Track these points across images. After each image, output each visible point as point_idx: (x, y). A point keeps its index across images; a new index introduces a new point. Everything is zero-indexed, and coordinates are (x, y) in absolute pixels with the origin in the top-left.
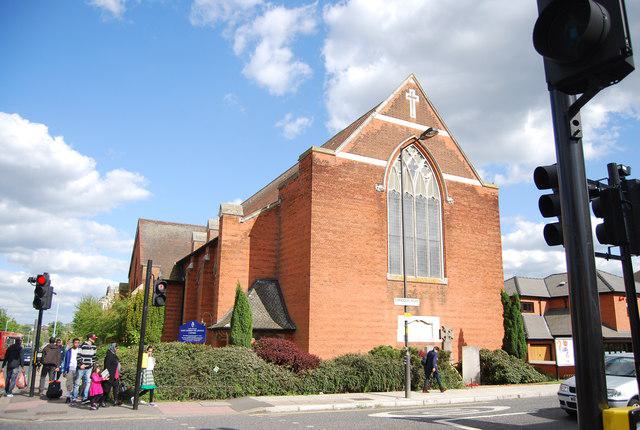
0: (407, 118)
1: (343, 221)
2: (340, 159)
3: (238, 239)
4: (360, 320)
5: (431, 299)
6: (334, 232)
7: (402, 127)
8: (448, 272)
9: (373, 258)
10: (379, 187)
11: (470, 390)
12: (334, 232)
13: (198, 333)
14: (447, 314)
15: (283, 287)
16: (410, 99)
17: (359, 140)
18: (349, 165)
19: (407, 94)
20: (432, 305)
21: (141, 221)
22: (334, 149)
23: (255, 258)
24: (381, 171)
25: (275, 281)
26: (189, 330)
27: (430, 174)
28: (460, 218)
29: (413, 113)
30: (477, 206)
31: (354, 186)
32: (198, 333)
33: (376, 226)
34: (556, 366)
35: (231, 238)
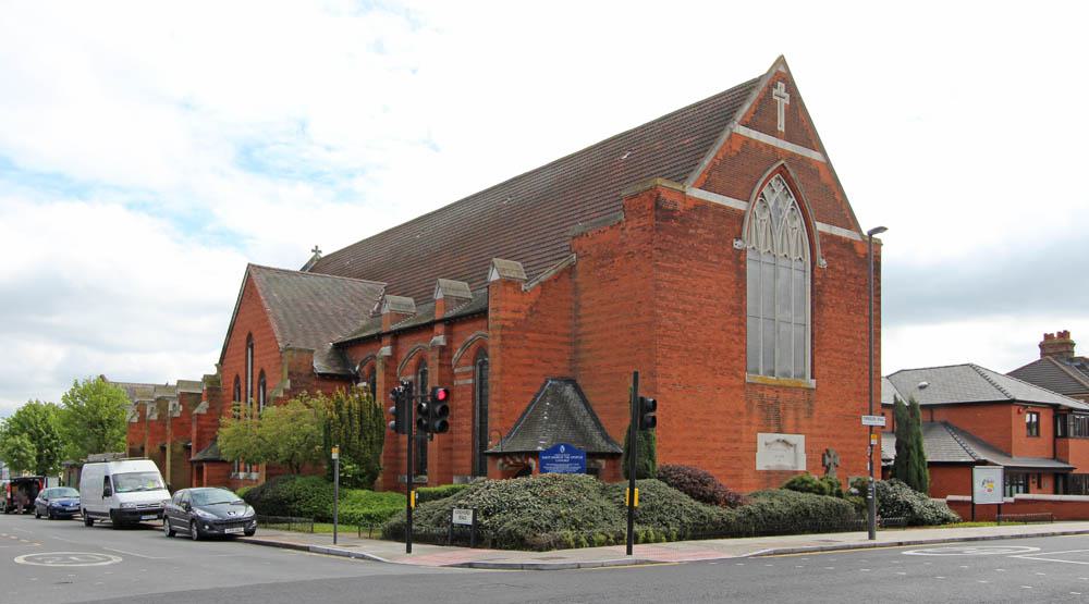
0: (773, 132)
1: (694, 295)
2: (691, 199)
3: (522, 316)
4: (714, 440)
5: (796, 410)
6: (685, 312)
7: (767, 146)
8: (816, 372)
9: (729, 350)
10: (738, 244)
11: (45, 523)
12: (685, 312)
13: (572, 461)
14: (816, 431)
15: (587, 391)
16: (778, 99)
17: (713, 167)
18: (702, 207)
19: (775, 91)
20: (797, 419)
21: (250, 266)
22: (681, 180)
24: (740, 217)
25: (572, 381)
26: (557, 457)
27: (799, 222)
28: (834, 290)
29: (781, 127)
30: (855, 271)
31: (707, 240)
32: (572, 461)
33: (733, 303)
34: (972, 503)
35: (513, 315)
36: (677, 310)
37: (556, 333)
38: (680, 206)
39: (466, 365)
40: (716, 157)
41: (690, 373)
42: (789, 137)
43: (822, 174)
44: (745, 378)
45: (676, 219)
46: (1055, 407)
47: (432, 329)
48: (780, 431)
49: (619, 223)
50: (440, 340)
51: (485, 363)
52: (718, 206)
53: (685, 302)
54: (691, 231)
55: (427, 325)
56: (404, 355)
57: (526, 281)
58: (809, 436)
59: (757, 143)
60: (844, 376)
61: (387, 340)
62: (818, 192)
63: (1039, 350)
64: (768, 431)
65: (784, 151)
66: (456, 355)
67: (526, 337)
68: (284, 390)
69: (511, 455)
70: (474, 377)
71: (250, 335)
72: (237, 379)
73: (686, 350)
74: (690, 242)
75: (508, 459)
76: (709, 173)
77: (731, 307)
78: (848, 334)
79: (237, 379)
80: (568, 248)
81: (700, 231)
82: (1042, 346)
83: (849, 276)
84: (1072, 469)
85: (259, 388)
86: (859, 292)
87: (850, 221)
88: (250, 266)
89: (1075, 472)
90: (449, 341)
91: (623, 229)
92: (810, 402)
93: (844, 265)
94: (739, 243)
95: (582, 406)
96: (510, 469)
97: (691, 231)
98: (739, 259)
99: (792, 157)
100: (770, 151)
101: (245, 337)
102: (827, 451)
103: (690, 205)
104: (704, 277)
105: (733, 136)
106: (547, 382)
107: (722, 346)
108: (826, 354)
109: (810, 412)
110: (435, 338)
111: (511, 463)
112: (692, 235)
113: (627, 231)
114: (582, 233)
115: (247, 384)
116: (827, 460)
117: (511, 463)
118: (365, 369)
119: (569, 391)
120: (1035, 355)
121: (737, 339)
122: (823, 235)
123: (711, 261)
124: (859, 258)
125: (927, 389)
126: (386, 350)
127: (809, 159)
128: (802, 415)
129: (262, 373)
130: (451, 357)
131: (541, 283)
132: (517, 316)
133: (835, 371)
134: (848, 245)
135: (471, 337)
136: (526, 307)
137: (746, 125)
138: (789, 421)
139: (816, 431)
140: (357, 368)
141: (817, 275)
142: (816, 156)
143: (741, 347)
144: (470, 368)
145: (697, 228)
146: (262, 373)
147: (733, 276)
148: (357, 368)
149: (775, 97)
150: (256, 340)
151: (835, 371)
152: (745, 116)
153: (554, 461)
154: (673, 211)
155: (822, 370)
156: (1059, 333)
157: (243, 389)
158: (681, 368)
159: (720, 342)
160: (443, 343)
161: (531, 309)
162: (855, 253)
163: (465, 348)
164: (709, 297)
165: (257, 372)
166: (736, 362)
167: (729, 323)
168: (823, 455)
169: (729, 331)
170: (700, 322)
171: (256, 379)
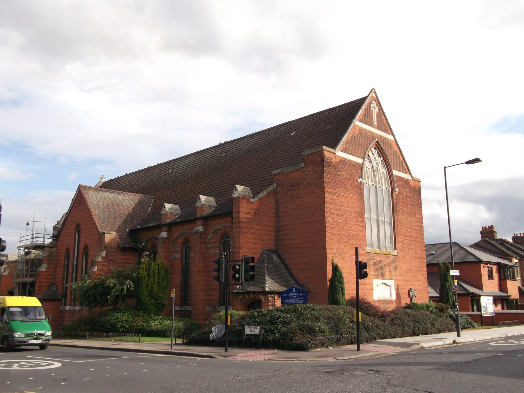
0: (372, 125)
2: (339, 157)
3: (250, 216)
5: (389, 267)
6: (338, 215)
12: (338, 215)
13: (299, 297)
14: (399, 278)
17: (347, 141)
18: (343, 161)
23: (371, 287)
24: (361, 167)
26: (291, 295)
29: (375, 123)
30: (410, 195)
31: (346, 178)
32: (299, 297)
36: (334, 214)
37: (267, 225)
38: (334, 160)
39: (216, 243)
40: (348, 137)
41: (341, 247)
42: (379, 128)
43: (393, 146)
44: (366, 250)
45: (332, 167)
46: (499, 265)
47: (195, 222)
48: (383, 278)
49: (302, 168)
50: (200, 229)
51: (187, 246)
52: (350, 161)
53: (338, 210)
54: (339, 173)
55: (193, 220)
56: (175, 236)
57: (253, 198)
58: (396, 280)
59: (365, 130)
60: (409, 249)
61: (199, 222)
62: (390, 155)
63: (480, 235)
64: (377, 278)
65: (377, 134)
66: (209, 237)
67: (253, 228)
68: (102, 257)
69: (248, 293)
70: (220, 250)
71: (78, 226)
72: (68, 250)
73: (339, 235)
74: (339, 179)
75: (246, 296)
76: (346, 144)
77: (358, 213)
78: (409, 227)
79: (68, 250)
80: (271, 180)
81: (343, 173)
82: (481, 233)
83: (406, 196)
84: (510, 296)
85: (83, 256)
86: (413, 205)
87: (407, 170)
88: (80, 185)
89: (511, 298)
90: (205, 229)
91: (304, 171)
92: (395, 262)
93: (406, 192)
94: (360, 179)
95: (282, 266)
96: (246, 301)
97: (339, 173)
98: (360, 188)
99: (381, 137)
100: (371, 134)
101: (74, 226)
102: (410, 288)
103: (338, 160)
104: (346, 197)
105: (355, 126)
106: (263, 252)
107: (355, 233)
108: (401, 237)
109: (396, 268)
110: (162, 233)
111: (248, 298)
112: (339, 175)
113: (306, 172)
114: (280, 173)
115: (74, 254)
116: (411, 294)
117: (248, 298)
118: (149, 245)
119: (275, 257)
120: (478, 238)
121: (361, 229)
122: (397, 177)
123: (348, 189)
124: (411, 188)
125: (433, 256)
126: (164, 234)
127: (388, 139)
128: (392, 270)
129: (86, 247)
130: (206, 238)
131: (260, 198)
132: (249, 216)
133: (405, 246)
134: (407, 181)
135: (218, 227)
136: (253, 211)
137: (360, 121)
138: (387, 273)
139: (399, 278)
140: (143, 244)
141: (394, 197)
142: (390, 137)
143: (364, 234)
144: (218, 244)
145: (342, 171)
146: (86, 247)
147: (356, 196)
148: (143, 244)
149: (372, 108)
150: (82, 228)
151: (405, 246)
152: (360, 116)
153: (289, 297)
154: (331, 163)
155: (399, 245)
156: (489, 226)
157: (71, 256)
158: (337, 245)
159: (354, 231)
160: (201, 230)
161: (255, 212)
162: (410, 185)
163: (215, 233)
164: (348, 207)
165: (82, 246)
166: (362, 241)
167: (357, 221)
168: (409, 291)
169: (357, 225)
170: (345, 220)
171: (81, 251)
